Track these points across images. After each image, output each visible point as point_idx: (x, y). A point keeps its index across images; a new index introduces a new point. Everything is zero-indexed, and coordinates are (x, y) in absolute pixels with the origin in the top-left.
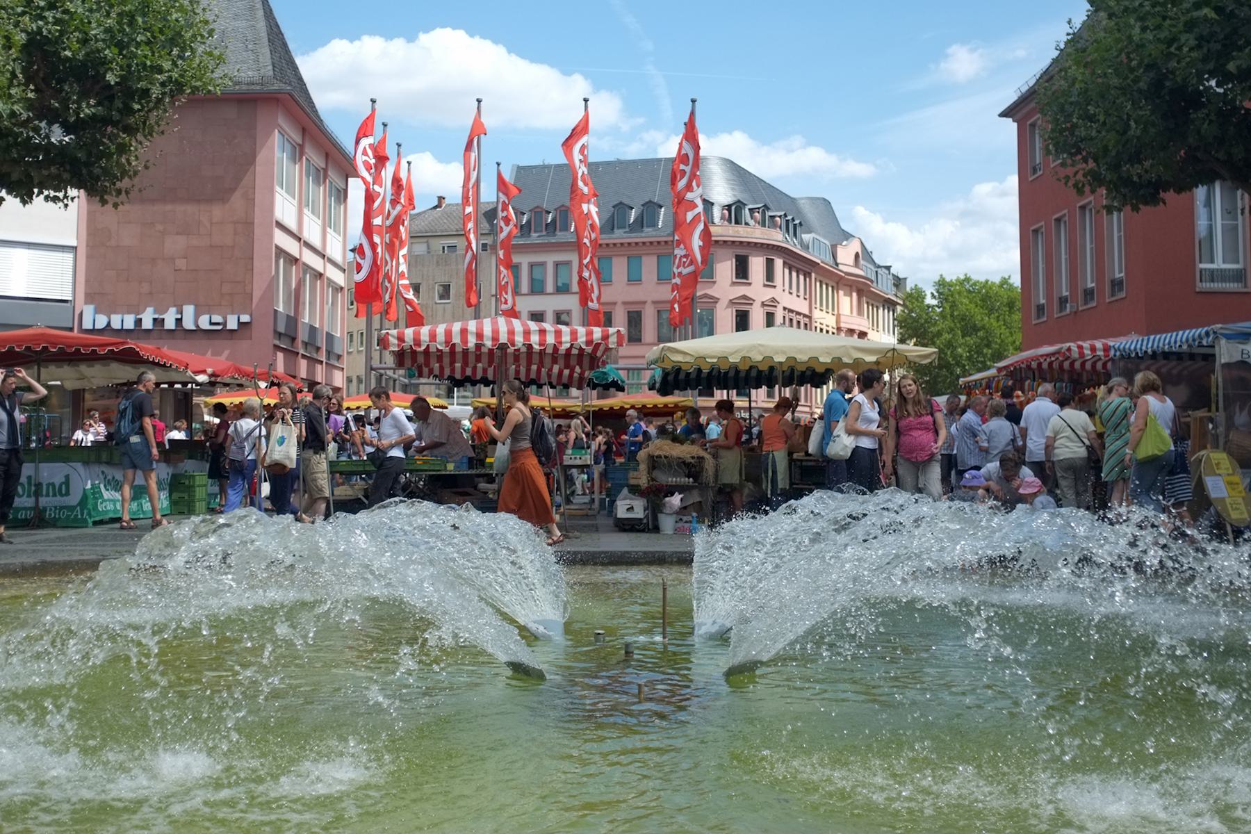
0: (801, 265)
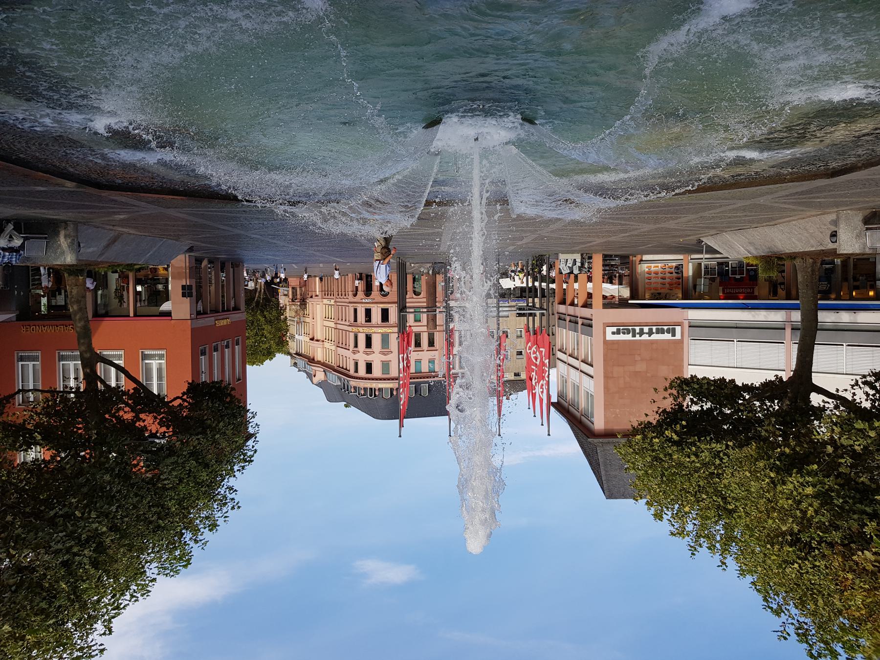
0: (341, 371)
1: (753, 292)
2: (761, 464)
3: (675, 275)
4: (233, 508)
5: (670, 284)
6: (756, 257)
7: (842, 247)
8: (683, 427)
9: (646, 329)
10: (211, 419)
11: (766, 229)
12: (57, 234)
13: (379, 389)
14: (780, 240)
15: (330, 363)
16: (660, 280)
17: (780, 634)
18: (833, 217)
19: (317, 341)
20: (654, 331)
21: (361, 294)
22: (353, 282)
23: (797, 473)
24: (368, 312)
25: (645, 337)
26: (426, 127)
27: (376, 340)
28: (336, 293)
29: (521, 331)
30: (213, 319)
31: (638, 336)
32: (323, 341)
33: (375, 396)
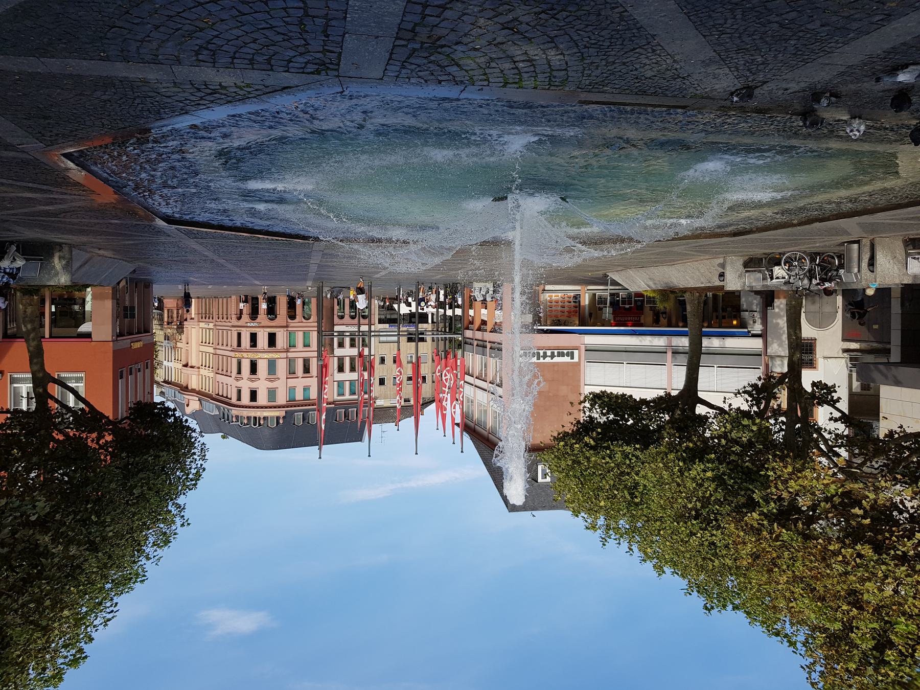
0: (221, 399)
1: (640, 320)
2: (671, 456)
3: (573, 304)
4: (183, 525)
5: (569, 312)
6: (654, 291)
7: (728, 285)
8: (598, 434)
9: (549, 353)
10: (173, 437)
11: (665, 268)
12: (51, 256)
13: (264, 418)
14: (676, 278)
15: (207, 391)
16: (559, 308)
17: (686, 591)
18: (721, 261)
19: (192, 367)
20: (556, 354)
21: (246, 318)
22: (238, 305)
23: (699, 462)
24: (253, 337)
25: (548, 360)
26: (495, 200)
27: (262, 367)
28: (215, 316)
29: (411, 357)
30: (129, 341)
31: (542, 358)
32: (199, 368)
33: (260, 425)
